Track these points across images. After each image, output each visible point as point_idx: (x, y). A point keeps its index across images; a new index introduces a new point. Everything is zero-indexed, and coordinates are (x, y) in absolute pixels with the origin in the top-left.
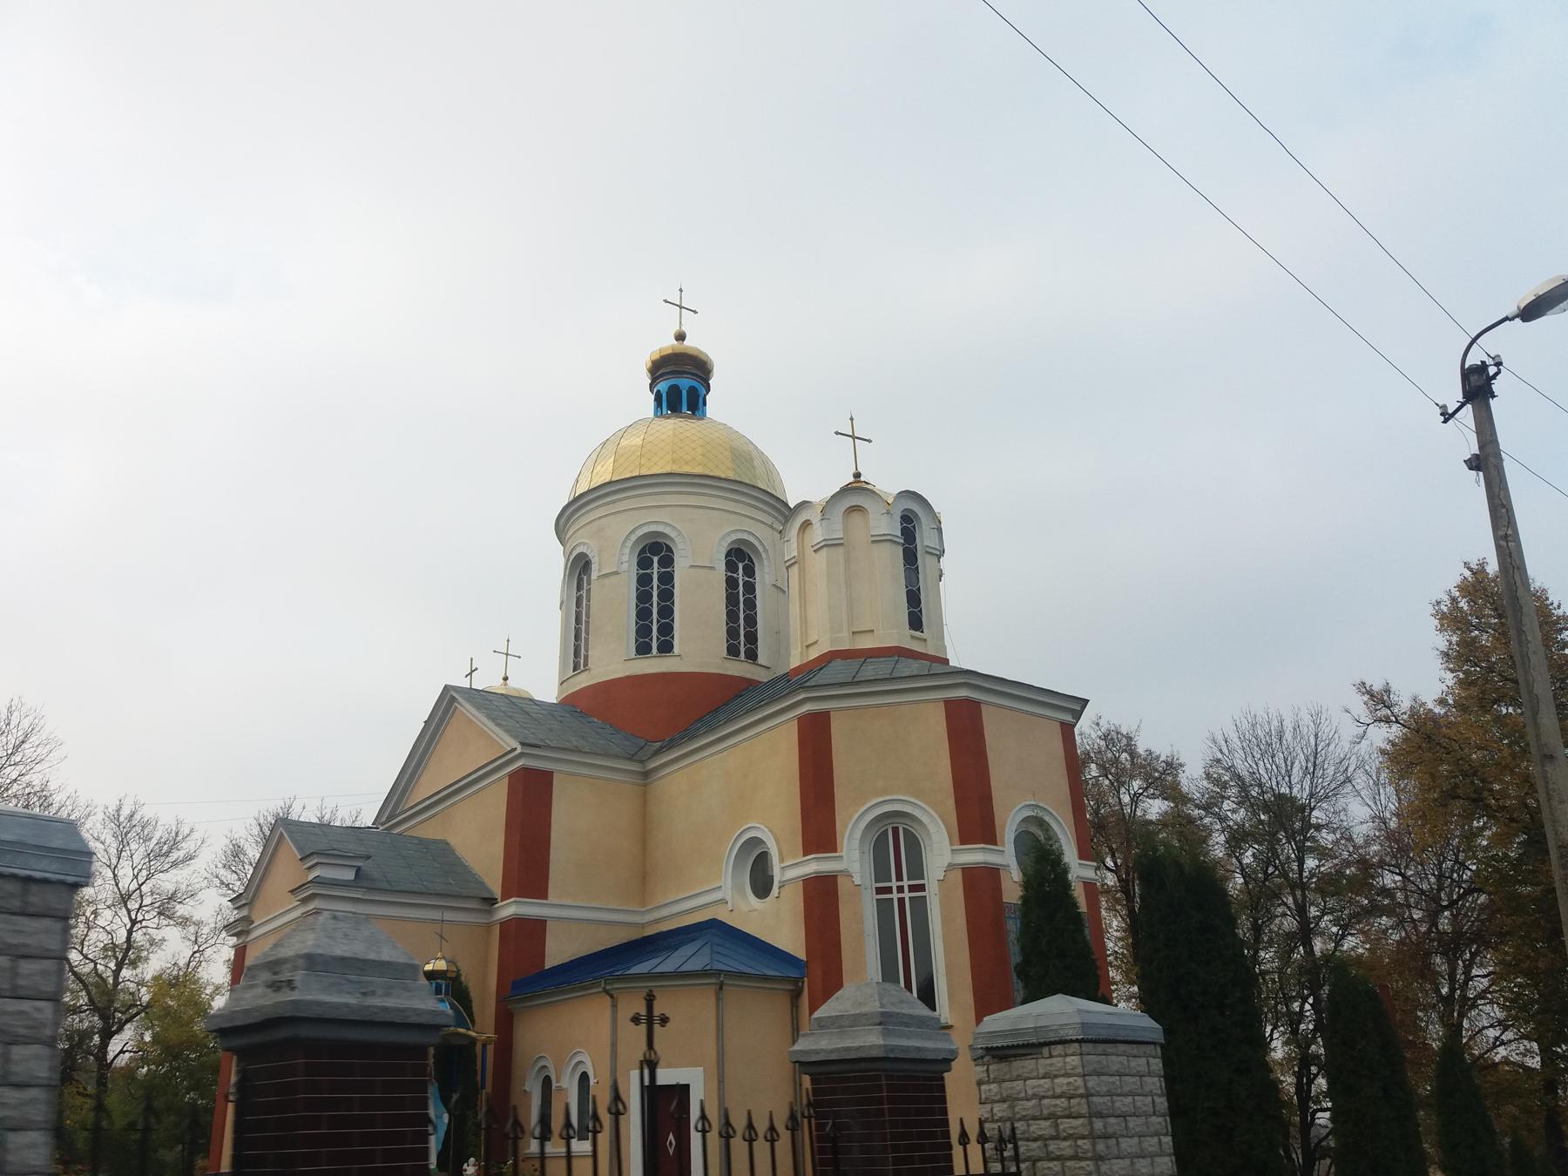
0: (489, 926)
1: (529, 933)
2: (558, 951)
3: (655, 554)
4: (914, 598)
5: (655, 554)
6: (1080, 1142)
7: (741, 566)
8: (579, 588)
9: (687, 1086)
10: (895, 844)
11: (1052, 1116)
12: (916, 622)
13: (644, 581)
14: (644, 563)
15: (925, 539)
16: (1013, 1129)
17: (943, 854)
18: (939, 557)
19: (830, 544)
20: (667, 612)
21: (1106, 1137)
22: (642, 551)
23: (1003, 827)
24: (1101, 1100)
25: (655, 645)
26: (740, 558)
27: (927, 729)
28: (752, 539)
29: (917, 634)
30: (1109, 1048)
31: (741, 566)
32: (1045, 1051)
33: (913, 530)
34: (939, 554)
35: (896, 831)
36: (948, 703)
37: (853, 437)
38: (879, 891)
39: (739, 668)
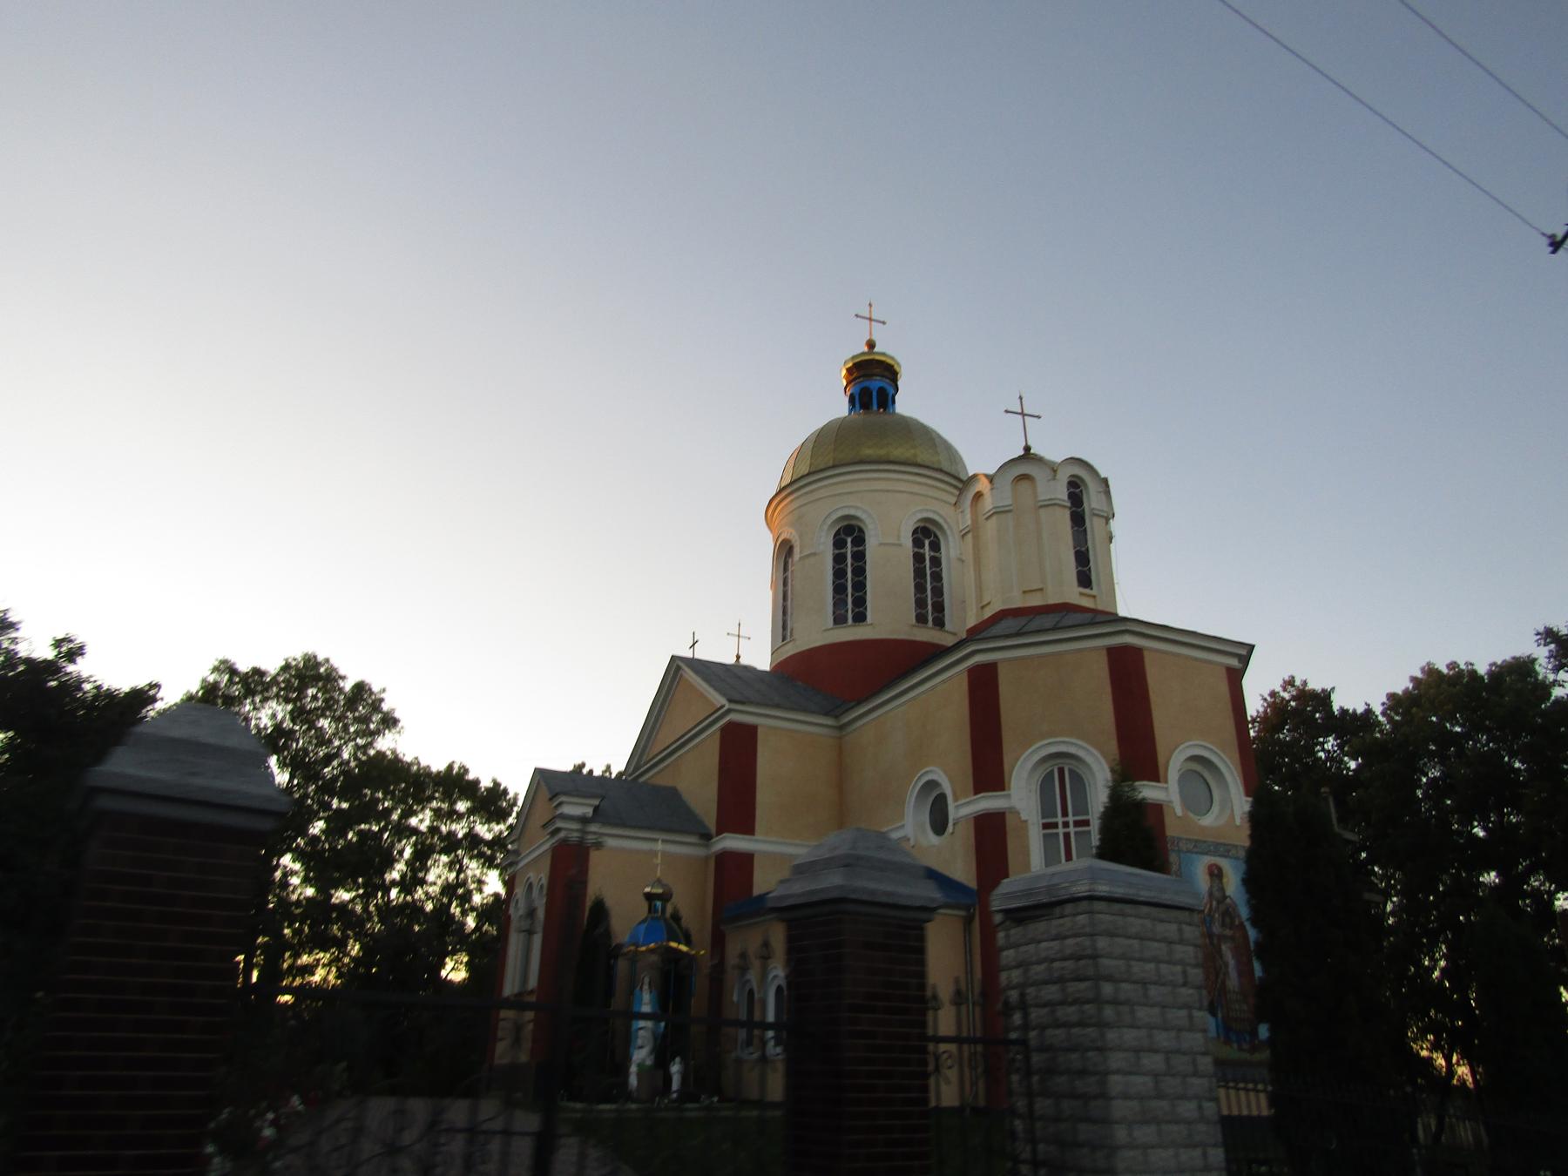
3: (850, 535)
4: (1082, 558)
5: (850, 535)
6: (1087, 1007)
7: (927, 542)
8: (785, 570)
9: (1252, 647)
10: (1061, 779)
11: (1061, 980)
12: (1085, 580)
13: (839, 559)
14: (839, 543)
15: (1092, 501)
16: (1022, 995)
18: (1107, 520)
19: (998, 512)
20: (860, 586)
21: (1115, 1002)
22: (915, 532)
24: (1113, 963)
26: (926, 534)
28: (936, 518)
29: (1087, 591)
30: (1128, 908)
31: (927, 542)
32: (1057, 910)
33: (1081, 499)
34: (1108, 517)
35: (1061, 771)
37: (1023, 414)
38: (1045, 826)
39: (927, 635)
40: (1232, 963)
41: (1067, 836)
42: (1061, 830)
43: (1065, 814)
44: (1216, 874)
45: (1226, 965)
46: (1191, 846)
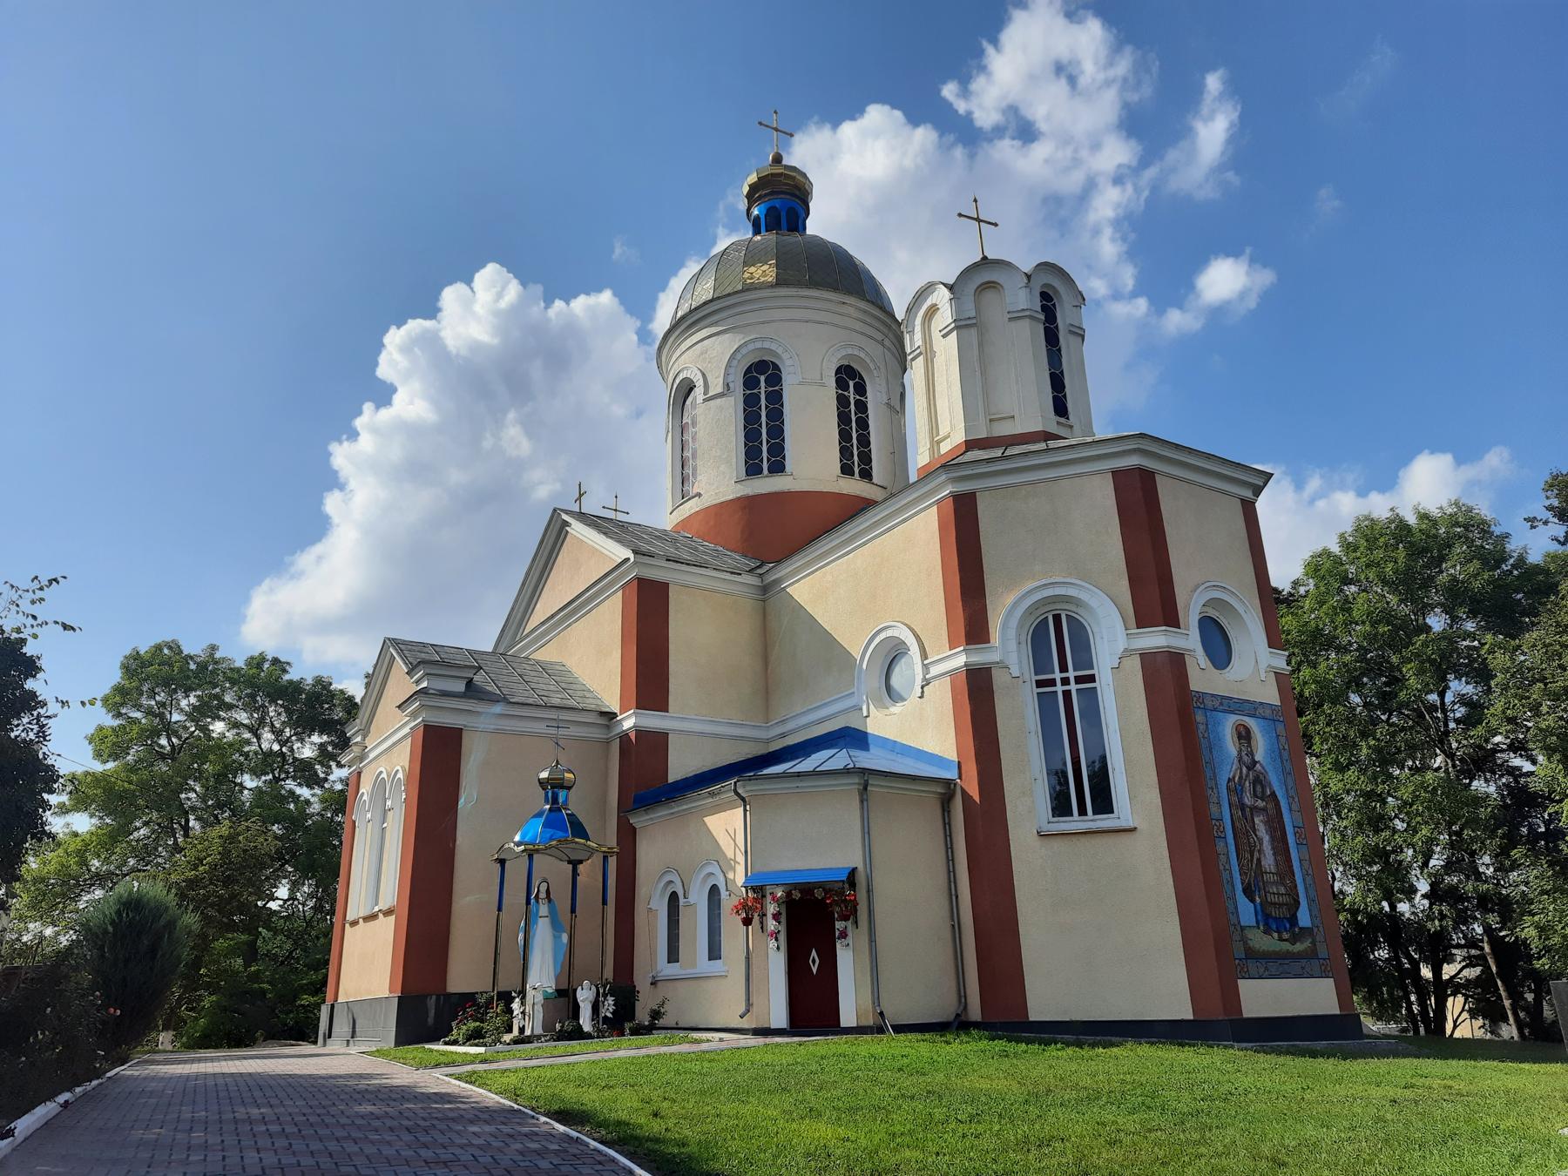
0: (608, 742)
1: (651, 746)
2: (680, 766)
4: (1057, 383)
7: (851, 384)
12: (1061, 408)
17: (1115, 642)
22: (838, 371)
23: (1187, 606)
25: (765, 465)
26: (848, 376)
27: (1094, 509)
29: (1062, 420)
31: (851, 384)
35: (1057, 618)
36: (1117, 474)
38: (1039, 684)
39: (854, 486)
40: (1266, 839)
41: (1067, 694)
42: (1059, 688)
43: (1063, 668)
44: (1244, 735)
45: (1260, 840)
46: (1216, 704)
